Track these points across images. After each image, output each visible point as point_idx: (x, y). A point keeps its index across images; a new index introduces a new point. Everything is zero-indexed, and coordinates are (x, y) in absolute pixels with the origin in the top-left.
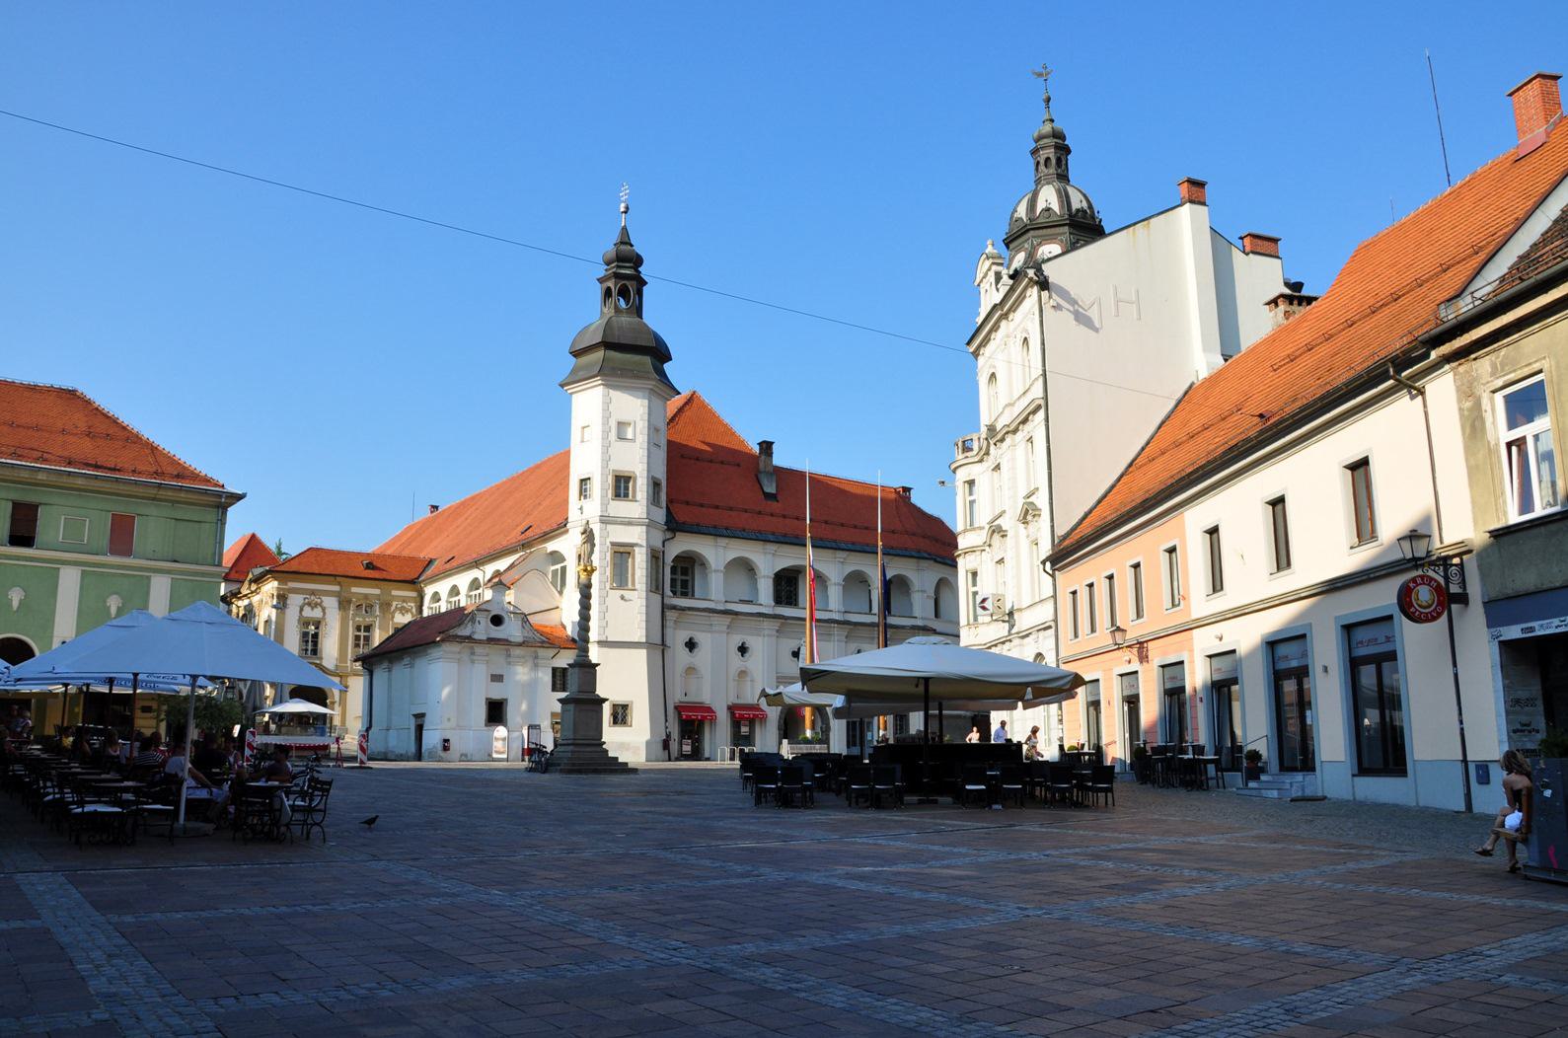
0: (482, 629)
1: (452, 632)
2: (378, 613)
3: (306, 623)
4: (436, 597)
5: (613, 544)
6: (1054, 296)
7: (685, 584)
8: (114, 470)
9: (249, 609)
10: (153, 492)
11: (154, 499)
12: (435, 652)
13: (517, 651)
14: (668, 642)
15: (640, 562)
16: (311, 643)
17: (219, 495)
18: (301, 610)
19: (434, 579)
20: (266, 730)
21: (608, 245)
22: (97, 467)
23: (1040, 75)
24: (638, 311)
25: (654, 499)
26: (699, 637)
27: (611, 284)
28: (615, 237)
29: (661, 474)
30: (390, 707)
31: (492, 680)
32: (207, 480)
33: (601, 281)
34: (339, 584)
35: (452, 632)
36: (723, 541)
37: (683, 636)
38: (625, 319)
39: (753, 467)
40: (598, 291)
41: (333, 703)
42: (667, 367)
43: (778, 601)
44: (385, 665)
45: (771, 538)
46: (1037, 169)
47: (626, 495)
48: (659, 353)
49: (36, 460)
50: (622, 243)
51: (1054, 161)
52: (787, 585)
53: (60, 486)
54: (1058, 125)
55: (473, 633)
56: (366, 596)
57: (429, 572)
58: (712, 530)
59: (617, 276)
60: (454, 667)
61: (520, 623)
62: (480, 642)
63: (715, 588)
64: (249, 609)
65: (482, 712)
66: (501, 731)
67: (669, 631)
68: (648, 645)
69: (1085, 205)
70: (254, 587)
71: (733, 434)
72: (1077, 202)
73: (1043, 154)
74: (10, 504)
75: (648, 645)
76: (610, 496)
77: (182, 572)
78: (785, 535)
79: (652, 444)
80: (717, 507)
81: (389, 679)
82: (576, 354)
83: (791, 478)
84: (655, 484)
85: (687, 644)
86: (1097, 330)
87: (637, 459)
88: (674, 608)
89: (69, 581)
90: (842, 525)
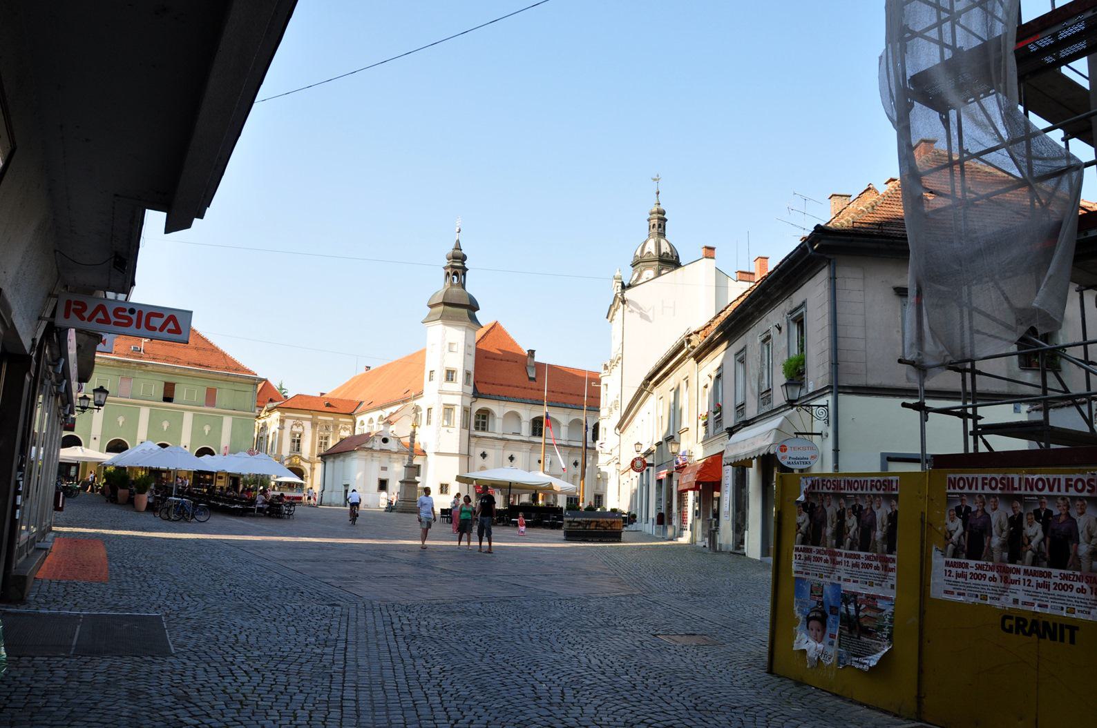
0: (378, 444)
1: (363, 446)
2: (332, 430)
3: (294, 434)
4: (362, 423)
5: (444, 404)
6: (630, 306)
7: (484, 424)
8: (207, 367)
9: (265, 425)
10: (225, 377)
11: (226, 381)
12: (355, 455)
13: (395, 456)
14: (472, 454)
15: (457, 414)
16: (297, 442)
17: (255, 379)
18: (292, 428)
19: (361, 413)
20: (274, 490)
21: (449, 249)
22: (200, 365)
23: (655, 180)
24: (463, 286)
25: (467, 382)
26: (488, 451)
27: (449, 271)
28: (453, 246)
29: (471, 368)
30: (333, 479)
31: (382, 470)
32: (249, 372)
33: (445, 268)
34: (312, 414)
35: (363, 446)
36: (503, 403)
37: (480, 451)
38: (455, 289)
39: (524, 362)
40: (443, 273)
41: (307, 477)
42: (477, 313)
43: (534, 434)
44: (332, 459)
45: (529, 401)
46: (650, 229)
47: (452, 380)
48: (472, 306)
49: (174, 363)
50: (456, 249)
51: (657, 226)
52: (537, 426)
53: (185, 375)
54: (662, 207)
55: (373, 446)
56: (326, 421)
57: (359, 409)
58: (497, 398)
59: (452, 267)
60: (363, 463)
61: (396, 442)
62: (376, 451)
63: (497, 427)
64: (265, 425)
65: (376, 485)
66: (384, 494)
67: (472, 449)
68: (460, 455)
69: (668, 250)
70: (267, 414)
71: (516, 344)
72: (665, 248)
73: (653, 222)
74: (163, 383)
75: (460, 455)
76: (444, 380)
77: (238, 415)
78: (537, 400)
79: (467, 354)
80: (502, 385)
81: (334, 465)
82: (431, 306)
83: (540, 367)
84: (468, 374)
85: (481, 455)
86: (650, 321)
87: (459, 361)
88: (475, 436)
89: (188, 418)
90: (571, 394)
